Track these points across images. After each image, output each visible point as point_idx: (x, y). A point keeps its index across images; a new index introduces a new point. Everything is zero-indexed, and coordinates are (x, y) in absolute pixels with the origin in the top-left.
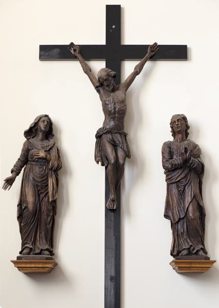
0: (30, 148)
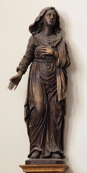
0: (36, 44)
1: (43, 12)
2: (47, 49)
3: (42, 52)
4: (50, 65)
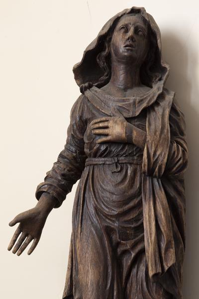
0: (86, 116)
3: (100, 135)
4: (124, 171)
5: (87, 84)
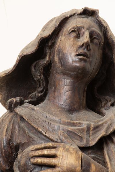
0: (18, 139)
1: (50, 26)
2: (58, 153)
5: (18, 99)
